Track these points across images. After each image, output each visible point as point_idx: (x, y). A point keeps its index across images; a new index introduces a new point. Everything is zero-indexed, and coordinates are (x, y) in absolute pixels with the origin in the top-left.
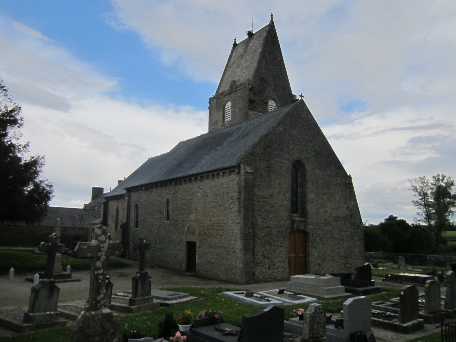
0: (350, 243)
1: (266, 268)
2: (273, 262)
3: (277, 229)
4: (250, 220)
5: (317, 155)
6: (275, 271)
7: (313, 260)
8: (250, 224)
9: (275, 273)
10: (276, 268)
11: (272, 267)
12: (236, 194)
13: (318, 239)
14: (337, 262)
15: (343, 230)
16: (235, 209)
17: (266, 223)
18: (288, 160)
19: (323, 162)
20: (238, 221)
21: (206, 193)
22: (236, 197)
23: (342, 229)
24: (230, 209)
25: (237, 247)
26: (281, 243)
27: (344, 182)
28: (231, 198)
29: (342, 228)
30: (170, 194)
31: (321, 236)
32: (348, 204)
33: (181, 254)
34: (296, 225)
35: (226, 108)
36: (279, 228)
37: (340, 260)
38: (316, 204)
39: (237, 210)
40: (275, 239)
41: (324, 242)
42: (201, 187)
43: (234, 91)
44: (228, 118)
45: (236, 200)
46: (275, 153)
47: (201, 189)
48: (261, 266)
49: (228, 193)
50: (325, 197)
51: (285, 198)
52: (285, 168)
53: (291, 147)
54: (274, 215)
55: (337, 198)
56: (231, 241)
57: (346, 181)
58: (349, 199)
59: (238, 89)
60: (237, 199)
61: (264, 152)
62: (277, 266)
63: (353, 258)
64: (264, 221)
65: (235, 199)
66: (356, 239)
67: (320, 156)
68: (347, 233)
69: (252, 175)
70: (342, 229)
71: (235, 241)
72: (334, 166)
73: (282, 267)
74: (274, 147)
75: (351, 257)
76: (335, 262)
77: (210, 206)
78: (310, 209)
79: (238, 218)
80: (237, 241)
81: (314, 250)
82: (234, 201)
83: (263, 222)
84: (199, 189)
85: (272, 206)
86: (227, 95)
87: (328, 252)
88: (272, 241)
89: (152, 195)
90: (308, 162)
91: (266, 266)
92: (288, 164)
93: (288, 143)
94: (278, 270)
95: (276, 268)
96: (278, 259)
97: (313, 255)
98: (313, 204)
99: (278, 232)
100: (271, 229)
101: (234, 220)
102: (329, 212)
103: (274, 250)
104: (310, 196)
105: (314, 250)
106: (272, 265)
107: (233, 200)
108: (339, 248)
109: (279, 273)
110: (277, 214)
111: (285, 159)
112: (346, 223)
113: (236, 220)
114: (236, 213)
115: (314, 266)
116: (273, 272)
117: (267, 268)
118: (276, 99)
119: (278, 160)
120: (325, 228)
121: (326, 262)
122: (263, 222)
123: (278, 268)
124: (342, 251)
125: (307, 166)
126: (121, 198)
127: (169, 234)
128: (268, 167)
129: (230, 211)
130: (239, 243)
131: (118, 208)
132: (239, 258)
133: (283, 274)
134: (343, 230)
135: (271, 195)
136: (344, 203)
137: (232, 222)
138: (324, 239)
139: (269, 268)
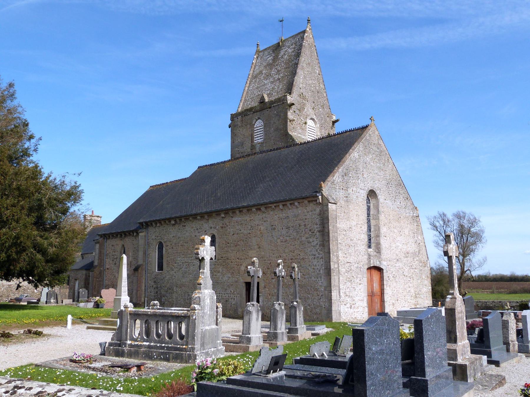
0: (419, 281)
1: (348, 308)
2: (354, 300)
3: (356, 265)
4: (335, 254)
5: (388, 185)
6: (356, 310)
7: (388, 299)
8: (335, 258)
9: (356, 313)
10: (356, 307)
11: (353, 306)
12: (318, 226)
13: (391, 276)
14: (408, 302)
15: (413, 267)
16: (315, 243)
17: (347, 257)
18: (364, 190)
19: (394, 193)
20: (321, 256)
21: (272, 226)
22: (317, 230)
23: (412, 266)
24: (309, 242)
25: (320, 284)
26: (360, 280)
27: (412, 215)
28: (310, 230)
29: (411, 265)
30: (215, 228)
31: (393, 273)
32: (416, 239)
33: (235, 298)
34: (372, 261)
35: (255, 127)
36: (358, 264)
37: (411, 299)
38: (388, 238)
39: (319, 244)
40: (355, 275)
41: (397, 279)
42: (265, 219)
43: (268, 107)
44: (258, 139)
45: (317, 232)
46: (352, 181)
47: (265, 221)
48: (343, 305)
49: (305, 225)
50: (396, 231)
51: (361, 231)
52: (361, 198)
53: (365, 176)
54: (353, 249)
55: (406, 231)
56: (311, 278)
57: (413, 214)
58: (416, 233)
59: (272, 106)
60: (319, 231)
61: (343, 181)
62: (357, 305)
63: (422, 298)
64: (345, 256)
65: (315, 232)
66: (424, 277)
67: (391, 185)
68: (416, 270)
69: (238, 210)
70: (412, 266)
71: (318, 278)
72: (403, 197)
73: (362, 307)
74: (350, 175)
75: (420, 298)
76: (407, 302)
77: (279, 240)
78: (384, 243)
79: (321, 252)
80: (321, 277)
81: (388, 288)
82: (314, 234)
83: (344, 257)
84: (263, 221)
85: (351, 240)
86: (257, 112)
87: (401, 291)
88: (352, 278)
89: (186, 229)
90: (380, 192)
91: (348, 305)
92: (364, 194)
93: (363, 171)
94: (358, 310)
95: (356, 307)
96: (358, 298)
97: (388, 294)
98: (386, 238)
99: (357, 268)
100: (351, 264)
101: (315, 255)
102: (400, 247)
103: (355, 288)
104: (384, 230)
105: (388, 288)
106: (353, 304)
107: (314, 232)
108: (409, 287)
109: (359, 312)
110: (356, 248)
111: (361, 189)
112: (415, 259)
113: (317, 255)
114: (318, 246)
115: (389, 306)
116: (354, 312)
117: (349, 307)
118: (315, 119)
119: (355, 189)
120: (397, 265)
121: (399, 302)
122: (344, 257)
123: (358, 308)
124: (412, 291)
125: (380, 197)
126: (130, 235)
127: (216, 275)
128: (347, 197)
129: (309, 245)
130: (323, 280)
131: (123, 246)
132: (323, 296)
133: (363, 314)
134: (413, 267)
135: (350, 228)
136: (413, 237)
137: (313, 257)
138: (396, 276)
139: (351, 307)
